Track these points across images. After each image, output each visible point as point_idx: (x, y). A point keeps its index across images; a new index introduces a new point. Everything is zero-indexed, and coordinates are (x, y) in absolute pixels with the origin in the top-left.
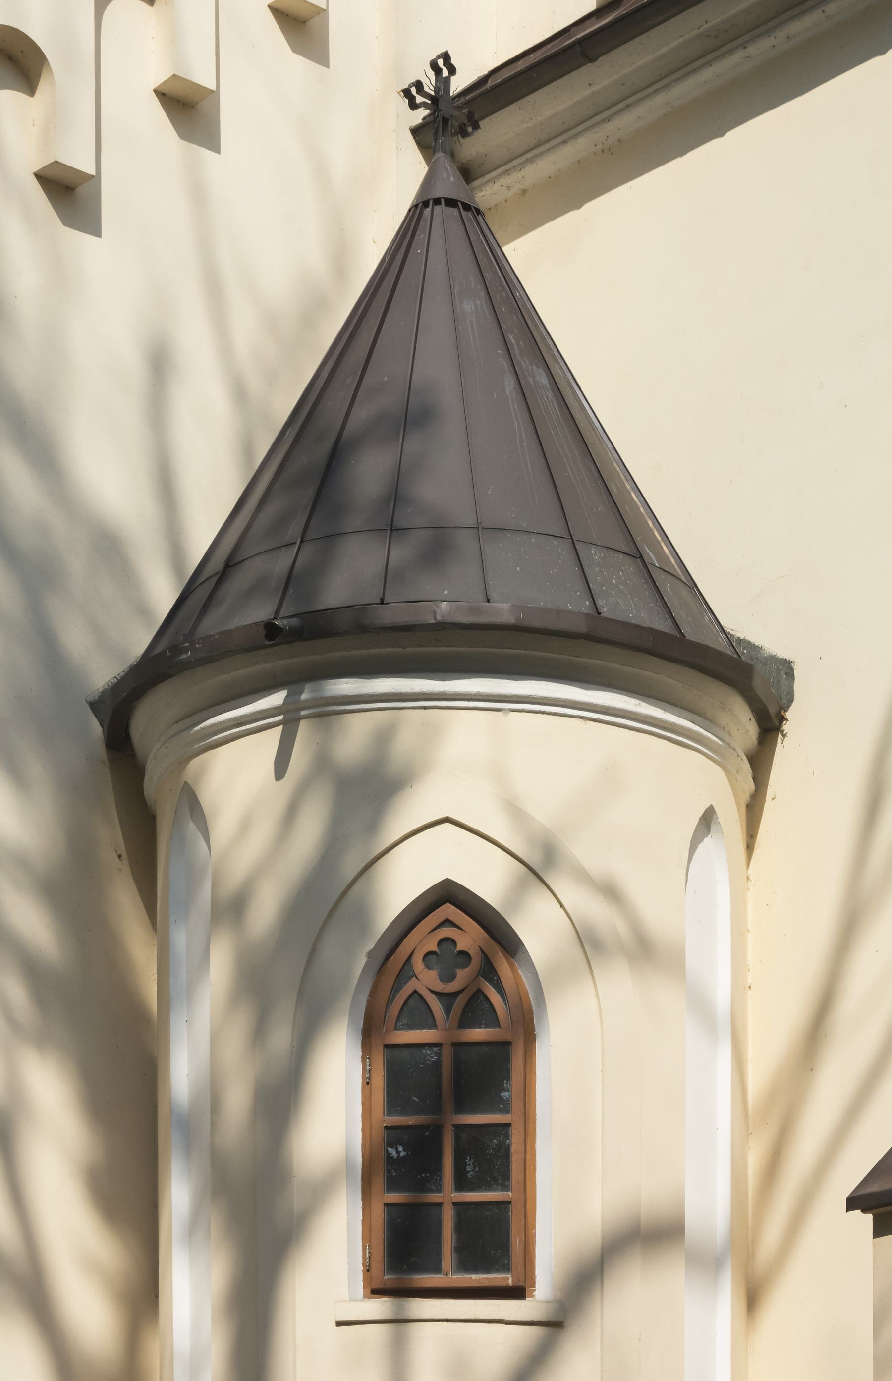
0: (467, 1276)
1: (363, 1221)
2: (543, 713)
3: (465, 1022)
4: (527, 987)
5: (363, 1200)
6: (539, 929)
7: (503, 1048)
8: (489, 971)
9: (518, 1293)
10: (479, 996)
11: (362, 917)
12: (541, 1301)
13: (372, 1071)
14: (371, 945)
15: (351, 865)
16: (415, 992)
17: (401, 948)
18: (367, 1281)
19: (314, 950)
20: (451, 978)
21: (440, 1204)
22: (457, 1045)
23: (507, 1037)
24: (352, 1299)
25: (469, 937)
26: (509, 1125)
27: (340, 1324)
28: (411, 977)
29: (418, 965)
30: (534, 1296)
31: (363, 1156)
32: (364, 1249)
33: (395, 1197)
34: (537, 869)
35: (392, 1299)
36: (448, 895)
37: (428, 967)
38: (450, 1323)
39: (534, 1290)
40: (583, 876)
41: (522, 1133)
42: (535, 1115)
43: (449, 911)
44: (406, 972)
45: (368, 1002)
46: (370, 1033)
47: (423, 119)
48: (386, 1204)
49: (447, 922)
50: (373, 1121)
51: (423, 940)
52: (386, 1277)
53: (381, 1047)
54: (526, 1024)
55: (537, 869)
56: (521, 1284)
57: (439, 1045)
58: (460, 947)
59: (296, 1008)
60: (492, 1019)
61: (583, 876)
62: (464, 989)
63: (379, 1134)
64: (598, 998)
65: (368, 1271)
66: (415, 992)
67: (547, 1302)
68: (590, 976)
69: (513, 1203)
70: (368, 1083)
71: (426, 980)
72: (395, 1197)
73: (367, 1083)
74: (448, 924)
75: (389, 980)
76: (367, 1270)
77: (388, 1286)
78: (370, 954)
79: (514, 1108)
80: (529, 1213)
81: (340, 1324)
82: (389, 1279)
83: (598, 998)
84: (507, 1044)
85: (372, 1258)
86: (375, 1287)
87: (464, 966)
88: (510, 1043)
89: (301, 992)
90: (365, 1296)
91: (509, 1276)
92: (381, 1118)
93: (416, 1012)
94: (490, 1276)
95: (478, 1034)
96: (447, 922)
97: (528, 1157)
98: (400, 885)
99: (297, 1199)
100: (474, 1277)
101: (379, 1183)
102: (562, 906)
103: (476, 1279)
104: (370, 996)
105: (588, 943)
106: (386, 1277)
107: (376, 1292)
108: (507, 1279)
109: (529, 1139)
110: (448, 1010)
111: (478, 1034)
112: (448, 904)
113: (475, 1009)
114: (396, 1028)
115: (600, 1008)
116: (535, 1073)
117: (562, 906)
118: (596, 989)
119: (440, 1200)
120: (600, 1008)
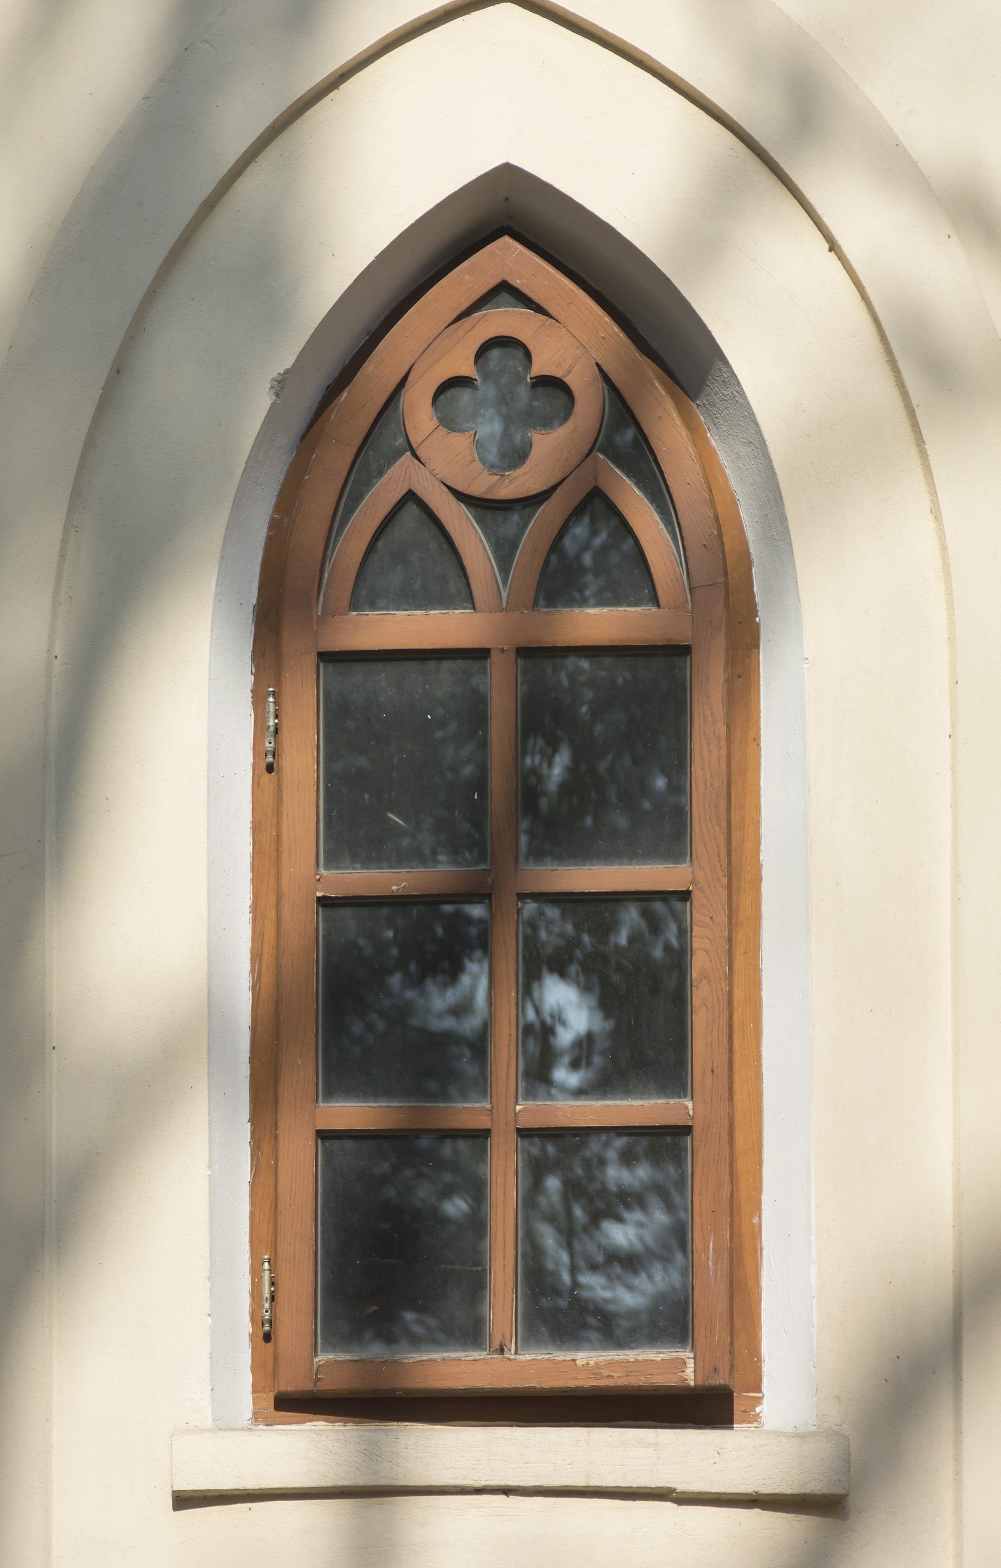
0: (561, 1356)
1: (253, 1184)
2: (318, 838)
3: (559, 582)
4: (735, 484)
5: (253, 1120)
6: (776, 323)
7: (666, 661)
8: (625, 440)
9: (708, 1407)
10: (596, 504)
11: (266, 273)
12: (779, 1434)
13: (285, 732)
14: (287, 360)
15: (239, 116)
16: (411, 496)
17: (369, 367)
18: (265, 1369)
19: (118, 372)
20: (516, 456)
21: (484, 1134)
22: (532, 655)
23: (681, 633)
24: (222, 1426)
25: (572, 338)
26: (685, 896)
27: (183, 1501)
28: (398, 454)
29: (419, 415)
30: (756, 1418)
31: (256, 988)
32: (255, 1272)
33: (350, 1113)
34: (768, 148)
35: (338, 1426)
36: (508, 213)
37: (448, 422)
38: (514, 1500)
39: (759, 1401)
40: (897, 166)
41: (723, 919)
42: (757, 866)
43: (507, 259)
44: (383, 436)
45: (274, 525)
46: (278, 617)
47: (758, 625)
48: (323, 1135)
49: (504, 291)
50: (285, 881)
51: (434, 343)
52: (322, 1358)
53: (312, 659)
54: (731, 610)
55: (768, 148)
56: (720, 1380)
57: (480, 655)
58: (538, 369)
59: (64, 542)
60: (630, 576)
61: (897, 166)
62: (554, 488)
63: (302, 923)
64: (938, 518)
65: (267, 1337)
66: (411, 496)
67: (802, 1436)
68: (914, 452)
69: (697, 1132)
70: (270, 768)
71: (445, 459)
72: (350, 1113)
73: (269, 766)
74: (505, 297)
75: (335, 459)
76: (266, 1337)
77: (330, 1383)
78: (281, 385)
79: (698, 845)
80: (741, 1163)
81: (183, 1501)
82: (332, 1365)
83: (938, 518)
84: (676, 653)
85: (283, 1284)
86: (292, 1383)
87: (547, 423)
88: (684, 650)
89: (77, 496)
90: (258, 1417)
91: (687, 1355)
92: (313, 875)
93: (414, 555)
94: (630, 1355)
95: (596, 622)
96: (504, 291)
97: (738, 994)
98: (382, 172)
99: (64, 1117)
100: (584, 1357)
101: (302, 1070)
102: (833, 247)
103: (589, 1364)
104: (278, 508)
105: (919, 370)
106: (322, 1358)
107: (293, 1403)
108: (677, 1365)
109: (740, 936)
110: (504, 552)
111: (596, 622)
112: (507, 239)
113: (580, 543)
114: (355, 605)
115: (944, 549)
116: (757, 740)
117: (833, 247)
118: (933, 493)
119: (482, 1122)
120: (944, 549)
